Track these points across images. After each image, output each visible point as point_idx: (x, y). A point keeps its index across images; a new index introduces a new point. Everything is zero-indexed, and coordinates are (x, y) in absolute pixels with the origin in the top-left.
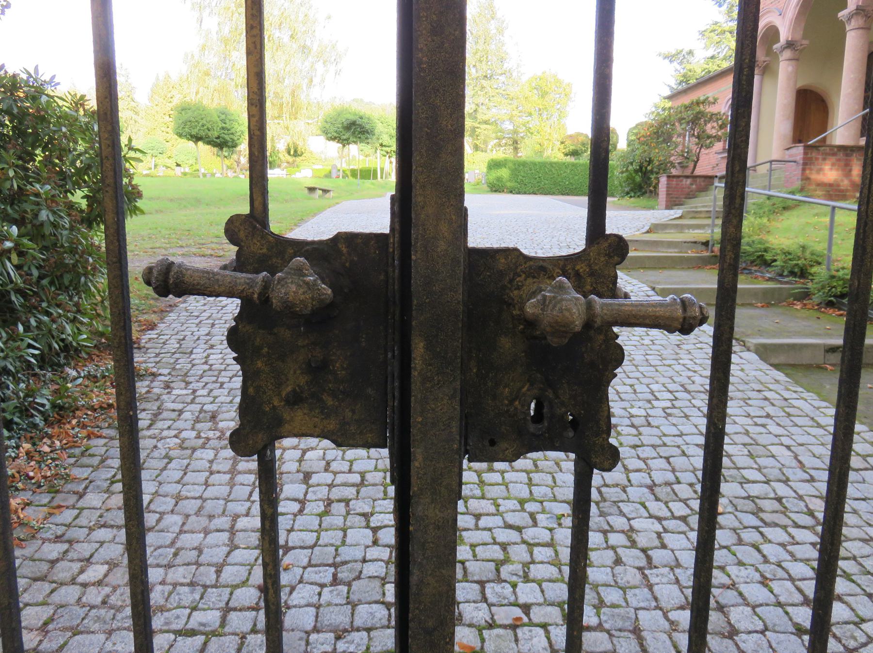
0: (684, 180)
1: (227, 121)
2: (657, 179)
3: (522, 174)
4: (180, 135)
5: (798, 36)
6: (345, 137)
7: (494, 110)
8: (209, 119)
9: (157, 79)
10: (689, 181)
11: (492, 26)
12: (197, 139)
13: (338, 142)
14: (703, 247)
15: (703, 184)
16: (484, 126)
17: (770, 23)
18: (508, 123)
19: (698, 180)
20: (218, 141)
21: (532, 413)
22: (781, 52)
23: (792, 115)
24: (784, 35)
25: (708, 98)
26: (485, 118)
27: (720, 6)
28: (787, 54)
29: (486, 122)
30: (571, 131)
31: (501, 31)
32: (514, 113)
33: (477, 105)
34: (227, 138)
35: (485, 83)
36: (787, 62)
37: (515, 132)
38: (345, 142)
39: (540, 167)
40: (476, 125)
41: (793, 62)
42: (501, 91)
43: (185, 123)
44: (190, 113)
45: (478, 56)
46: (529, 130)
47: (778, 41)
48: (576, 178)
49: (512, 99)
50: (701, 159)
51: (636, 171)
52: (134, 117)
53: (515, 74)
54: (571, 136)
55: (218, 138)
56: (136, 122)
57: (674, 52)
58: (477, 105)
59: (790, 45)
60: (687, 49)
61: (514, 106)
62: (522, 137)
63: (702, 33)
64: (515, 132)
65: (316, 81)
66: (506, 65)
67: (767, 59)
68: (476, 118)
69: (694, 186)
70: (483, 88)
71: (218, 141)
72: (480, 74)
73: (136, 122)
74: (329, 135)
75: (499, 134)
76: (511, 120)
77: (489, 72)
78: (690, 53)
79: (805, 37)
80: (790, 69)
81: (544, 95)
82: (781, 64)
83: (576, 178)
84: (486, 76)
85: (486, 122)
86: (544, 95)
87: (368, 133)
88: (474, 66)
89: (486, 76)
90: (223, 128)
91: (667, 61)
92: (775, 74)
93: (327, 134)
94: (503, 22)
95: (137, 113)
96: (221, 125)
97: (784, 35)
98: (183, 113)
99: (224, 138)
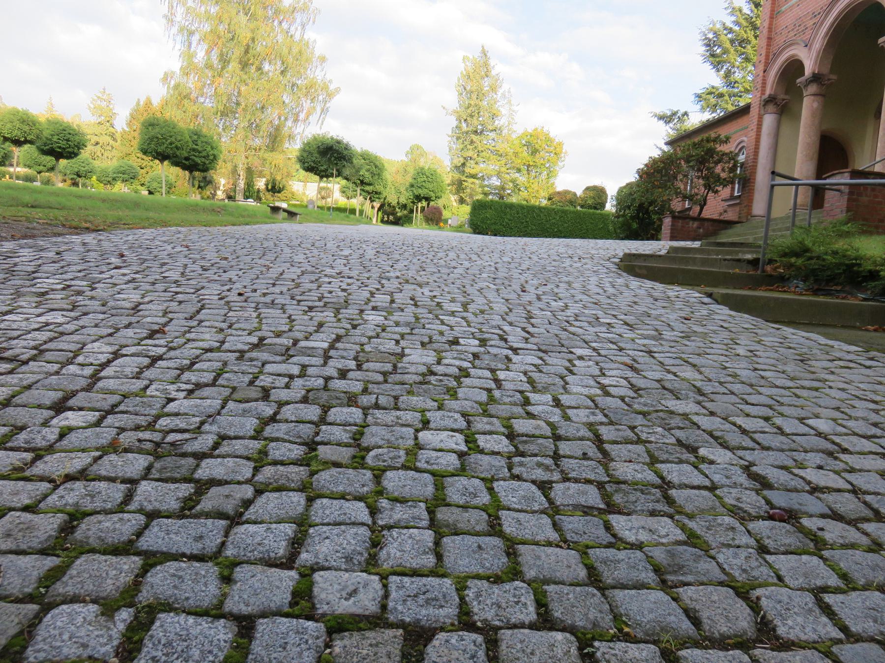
0: (691, 223)
1: (199, 142)
2: (660, 220)
3: (508, 217)
4: (145, 152)
5: (825, 70)
6: (322, 168)
7: (482, 165)
8: (179, 138)
9: (138, 103)
10: (696, 224)
11: (486, 84)
12: (162, 157)
13: (315, 174)
14: (750, 267)
15: (711, 228)
16: (472, 180)
17: (793, 56)
18: (495, 178)
19: (706, 224)
20: (187, 163)
21: (697, 244)
22: (806, 86)
23: (816, 156)
24: (809, 68)
25: (720, 135)
26: (473, 172)
27: (718, 71)
28: (813, 88)
29: (473, 176)
30: (560, 188)
31: (494, 89)
32: (503, 169)
33: (465, 158)
34: (198, 160)
35: (475, 138)
36: (812, 97)
37: (503, 188)
38: (324, 175)
39: (528, 211)
40: (464, 178)
41: (819, 98)
42: (491, 148)
43: (151, 139)
44: (157, 129)
45: (469, 111)
46: (516, 186)
47: (804, 74)
48: (566, 225)
49: (501, 156)
50: (708, 202)
51: (632, 218)
52: (111, 142)
53: (505, 132)
54: (559, 193)
55: (187, 159)
56: (112, 147)
57: (669, 113)
58: (465, 158)
59: (816, 78)
60: (682, 111)
61: (503, 162)
62: (509, 194)
63: (699, 96)
64: (503, 188)
65: (302, 116)
66: (497, 122)
67: (787, 97)
68: (464, 171)
69: (701, 230)
70: (472, 142)
71: (187, 163)
72: (470, 129)
73: (112, 147)
74: (306, 165)
75: (486, 189)
76: (499, 175)
77: (480, 127)
78: (686, 114)
79: (832, 71)
80: (815, 105)
81: (535, 152)
82: (805, 99)
83: (566, 225)
84: (476, 132)
85: (473, 176)
86: (535, 152)
87: (345, 159)
88: (465, 120)
89: (476, 132)
90: (194, 150)
91: (661, 122)
92: (797, 117)
93: (304, 163)
94: (497, 80)
95: (115, 140)
96: (191, 145)
97: (809, 68)
98: (150, 128)
99: (193, 160)
